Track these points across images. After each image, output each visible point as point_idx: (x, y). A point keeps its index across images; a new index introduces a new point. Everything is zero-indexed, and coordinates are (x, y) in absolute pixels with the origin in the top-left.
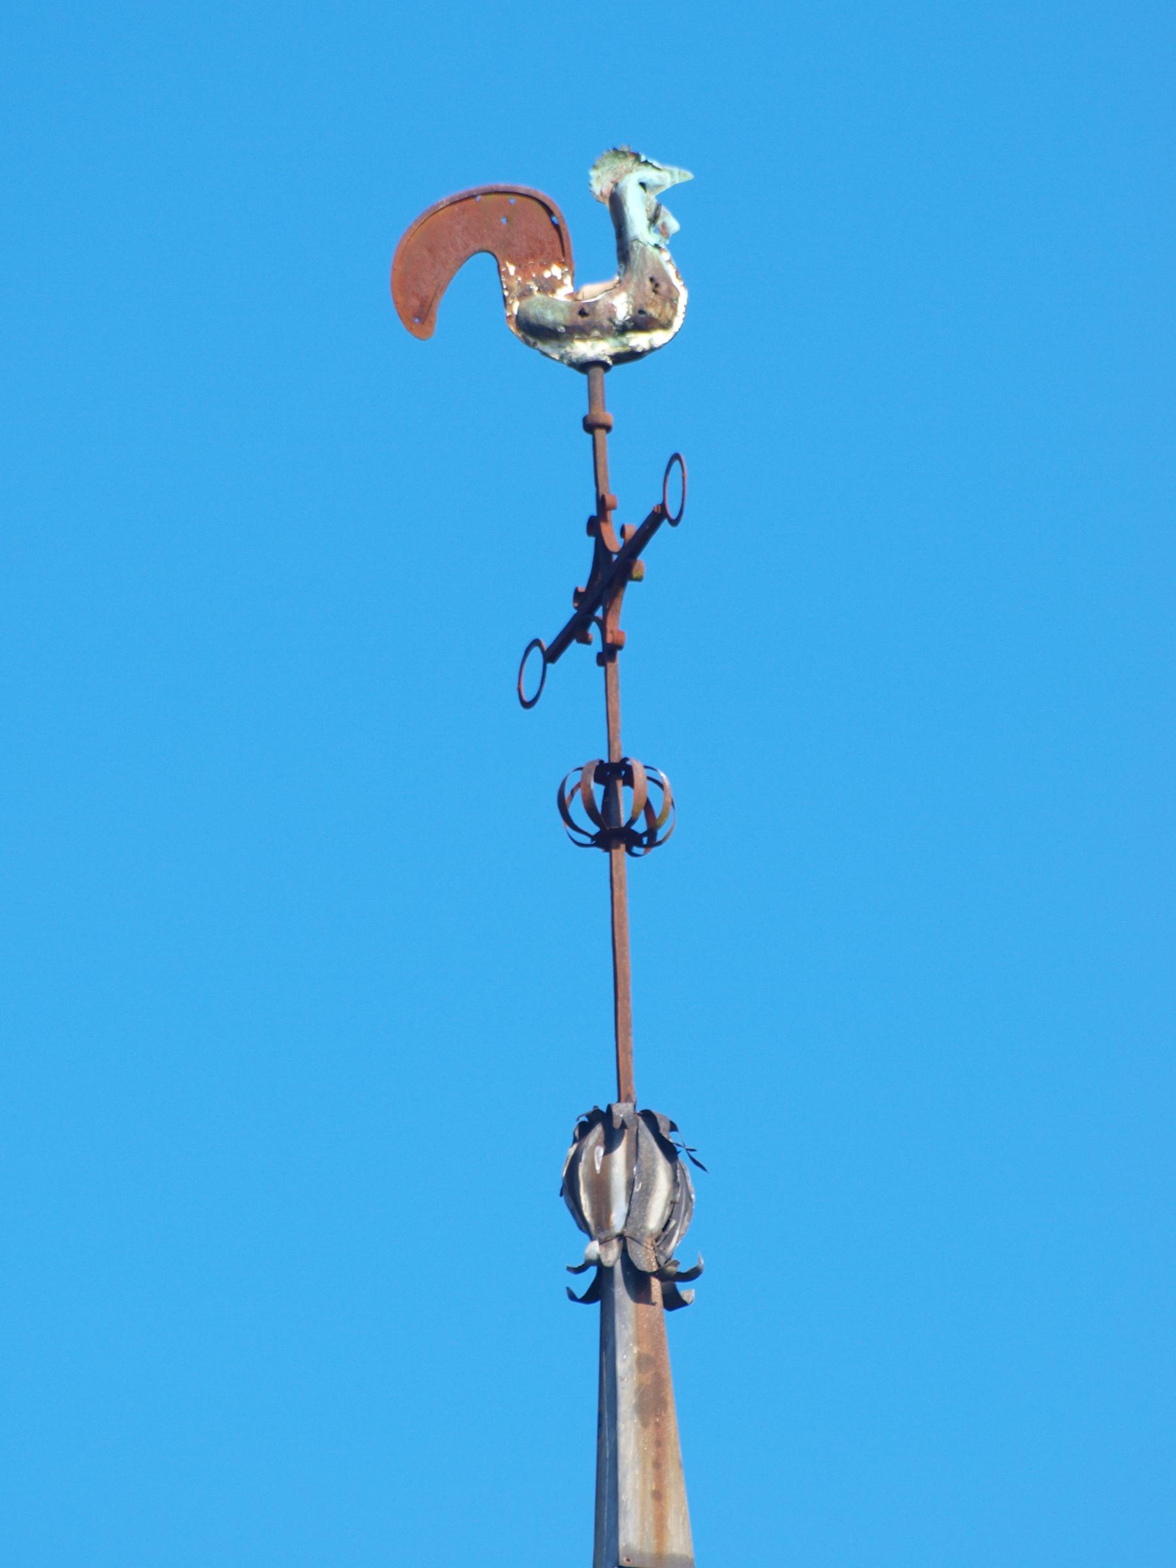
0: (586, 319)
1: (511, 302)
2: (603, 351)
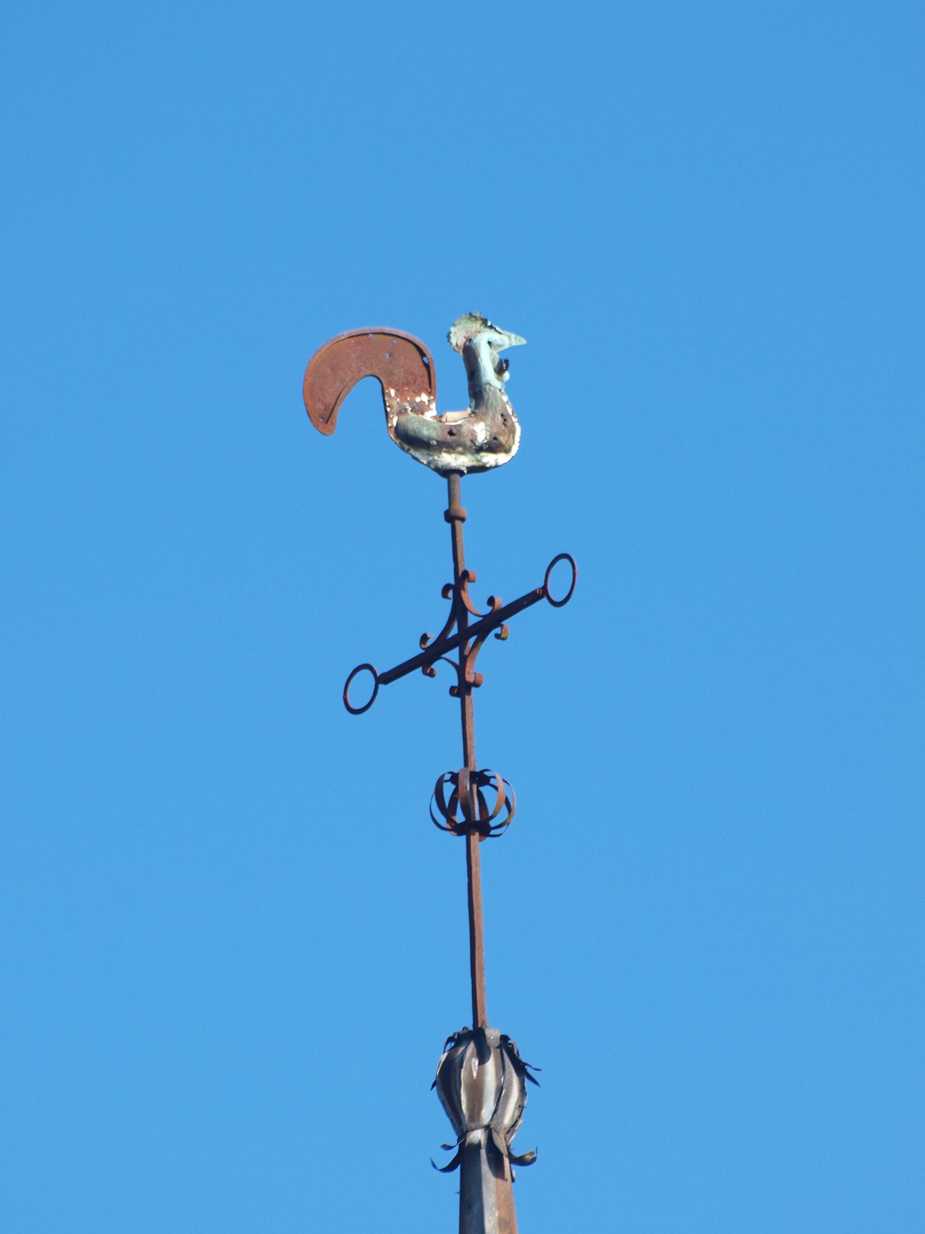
0: (453, 438)
1: (391, 416)
2: (463, 463)
